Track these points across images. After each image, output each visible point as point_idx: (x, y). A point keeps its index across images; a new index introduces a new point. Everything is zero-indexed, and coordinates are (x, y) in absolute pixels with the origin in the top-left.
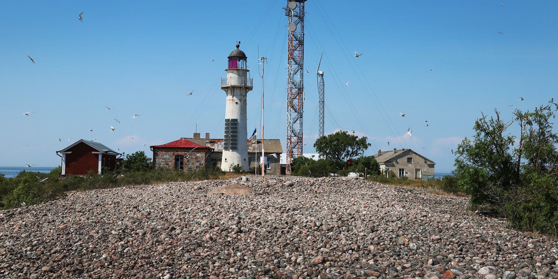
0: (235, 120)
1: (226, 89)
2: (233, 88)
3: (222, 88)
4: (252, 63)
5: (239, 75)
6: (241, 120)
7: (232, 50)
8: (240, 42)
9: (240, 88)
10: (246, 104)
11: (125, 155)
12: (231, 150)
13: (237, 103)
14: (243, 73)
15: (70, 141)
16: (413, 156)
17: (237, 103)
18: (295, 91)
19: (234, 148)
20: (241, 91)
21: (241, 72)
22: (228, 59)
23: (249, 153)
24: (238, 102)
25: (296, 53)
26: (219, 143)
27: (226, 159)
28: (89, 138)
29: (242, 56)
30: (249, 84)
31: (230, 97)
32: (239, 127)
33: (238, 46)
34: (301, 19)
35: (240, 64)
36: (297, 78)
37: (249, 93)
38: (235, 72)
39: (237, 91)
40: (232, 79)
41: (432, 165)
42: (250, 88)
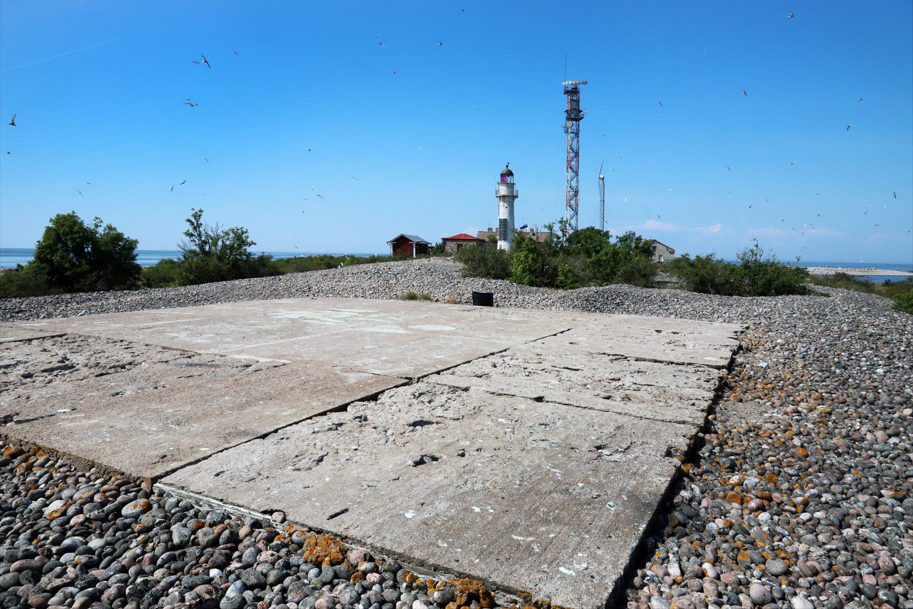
2: (504, 196)
4: (516, 179)
7: (503, 169)
11: (104, 225)
14: (511, 186)
15: (396, 235)
16: (657, 245)
18: (572, 193)
19: (505, 239)
20: (510, 199)
25: (573, 163)
28: (408, 233)
29: (510, 174)
31: (502, 203)
34: (577, 134)
35: (509, 179)
36: (574, 183)
37: (516, 201)
39: (507, 199)
40: (503, 190)
41: (672, 252)
42: (517, 197)
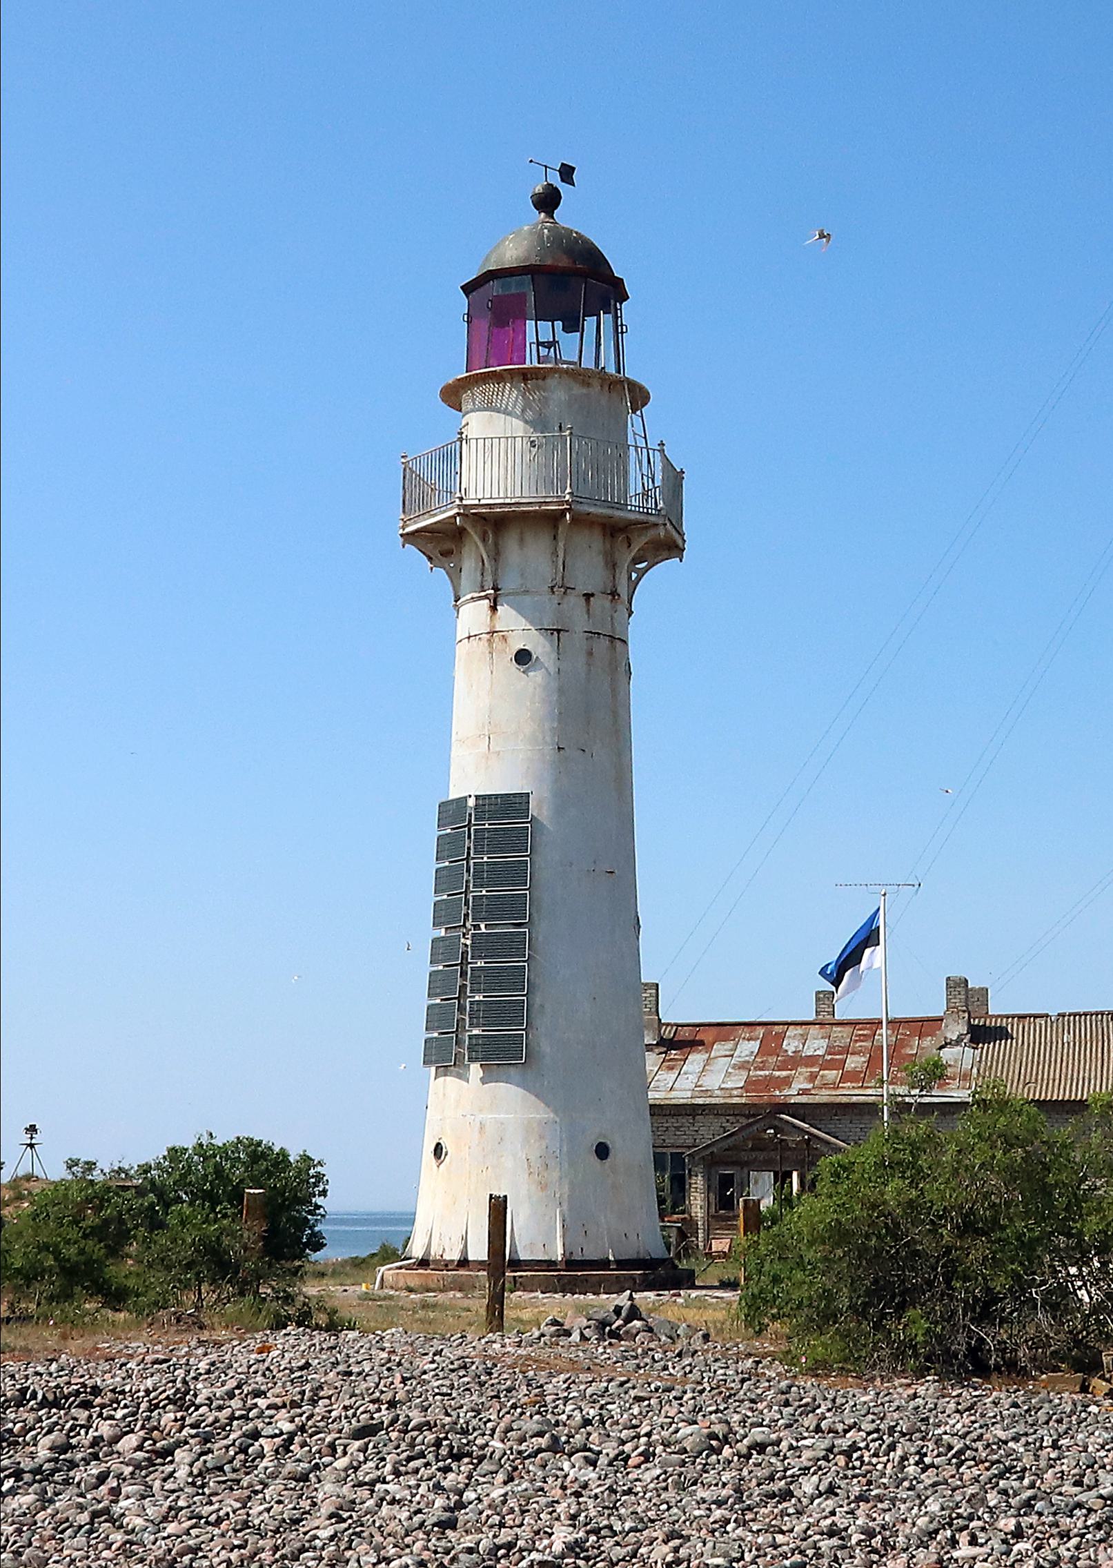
0: (513, 805)
1: (441, 543)
2: (495, 524)
3: (409, 538)
5: (539, 423)
6: (562, 800)
8: (567, 173)
9: (546, 521)
10: (619, 670)
12: (475, 1070)
13: (523, 657)
17: (523, 657)
21: (558, 393)
22: (462, 303)
23: (658, 1110)
24: (539, 645)
26: (719, 1049)
27: (438, 1150)
29: (575, 282)
30: (638, 486)
32: (552, 863)
33: (548, 201)
37: (658, 587)
38: (510, 395)
39: (529, 558)
40: (496, 457)
42: (672, 548)
